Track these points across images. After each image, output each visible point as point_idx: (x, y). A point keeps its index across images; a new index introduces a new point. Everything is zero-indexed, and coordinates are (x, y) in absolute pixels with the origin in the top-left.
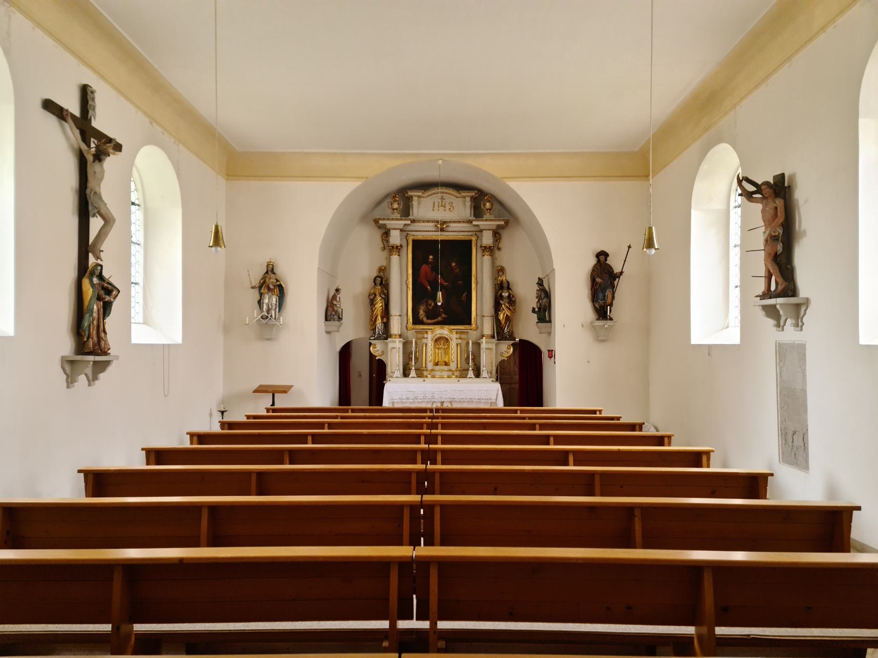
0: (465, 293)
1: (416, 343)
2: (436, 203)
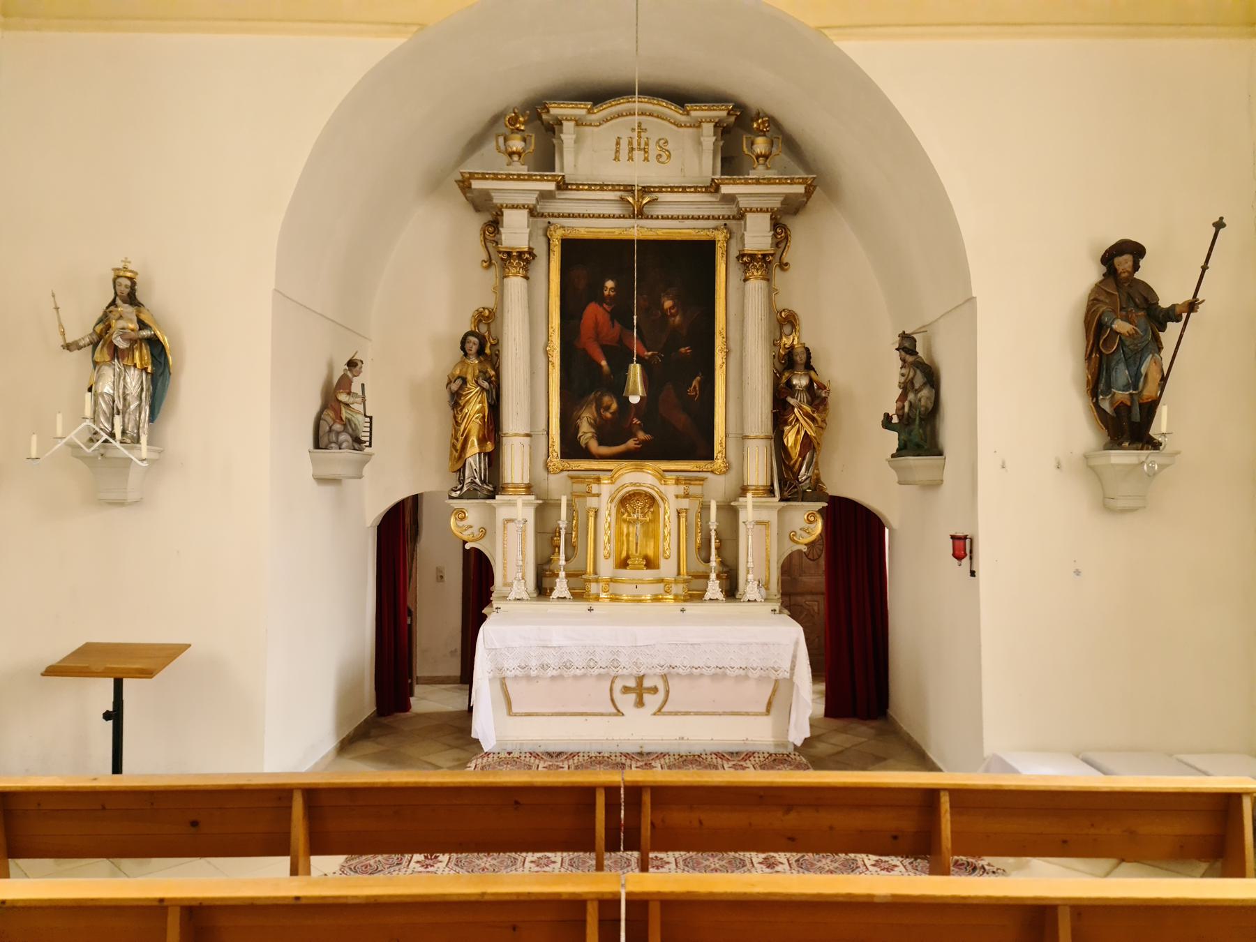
0: (698, 378)
1: (570, 506)
2: (621, 141)
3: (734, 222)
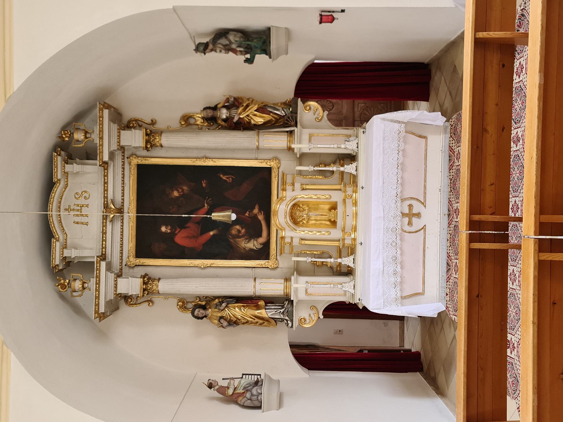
0: (221, 176)
1: (298, 255)
3: (126, 152)
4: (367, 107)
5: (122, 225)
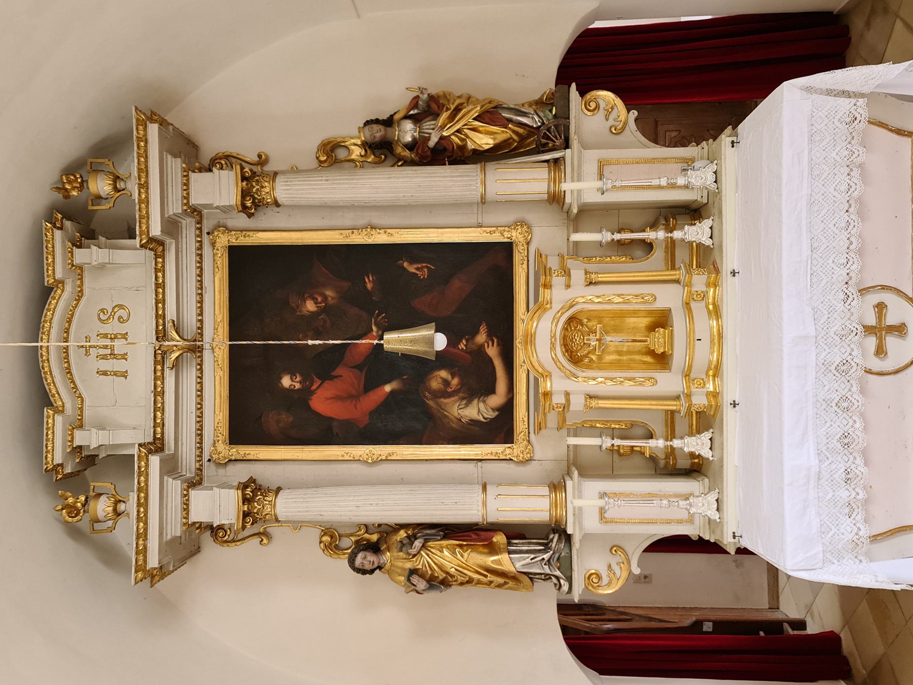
0: (406, 264)
3: (205, 222)
4: (683, 137)
5: (200, 375)
